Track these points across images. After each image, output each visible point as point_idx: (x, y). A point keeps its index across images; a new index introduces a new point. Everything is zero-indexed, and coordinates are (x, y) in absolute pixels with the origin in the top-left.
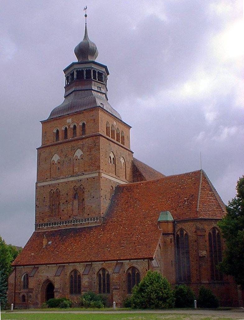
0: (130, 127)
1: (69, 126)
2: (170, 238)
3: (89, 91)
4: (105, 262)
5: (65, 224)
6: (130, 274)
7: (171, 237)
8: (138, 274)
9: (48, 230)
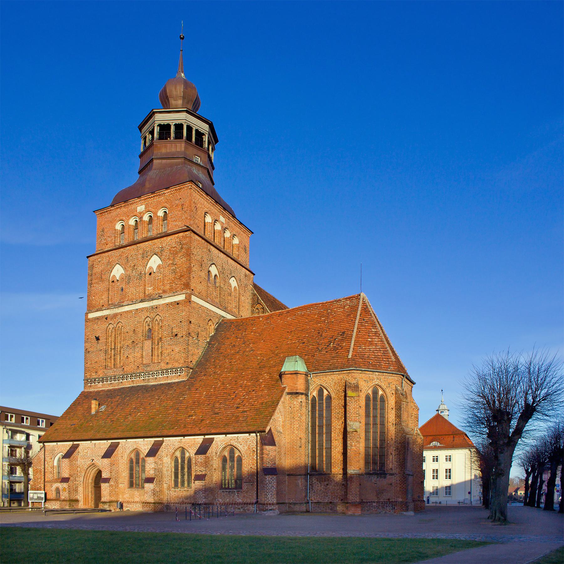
0: (275, 442)
1: (141, 218)
6: (369, 398)
7: (302, 398)
8: (240, 459)
9: (103, 389)
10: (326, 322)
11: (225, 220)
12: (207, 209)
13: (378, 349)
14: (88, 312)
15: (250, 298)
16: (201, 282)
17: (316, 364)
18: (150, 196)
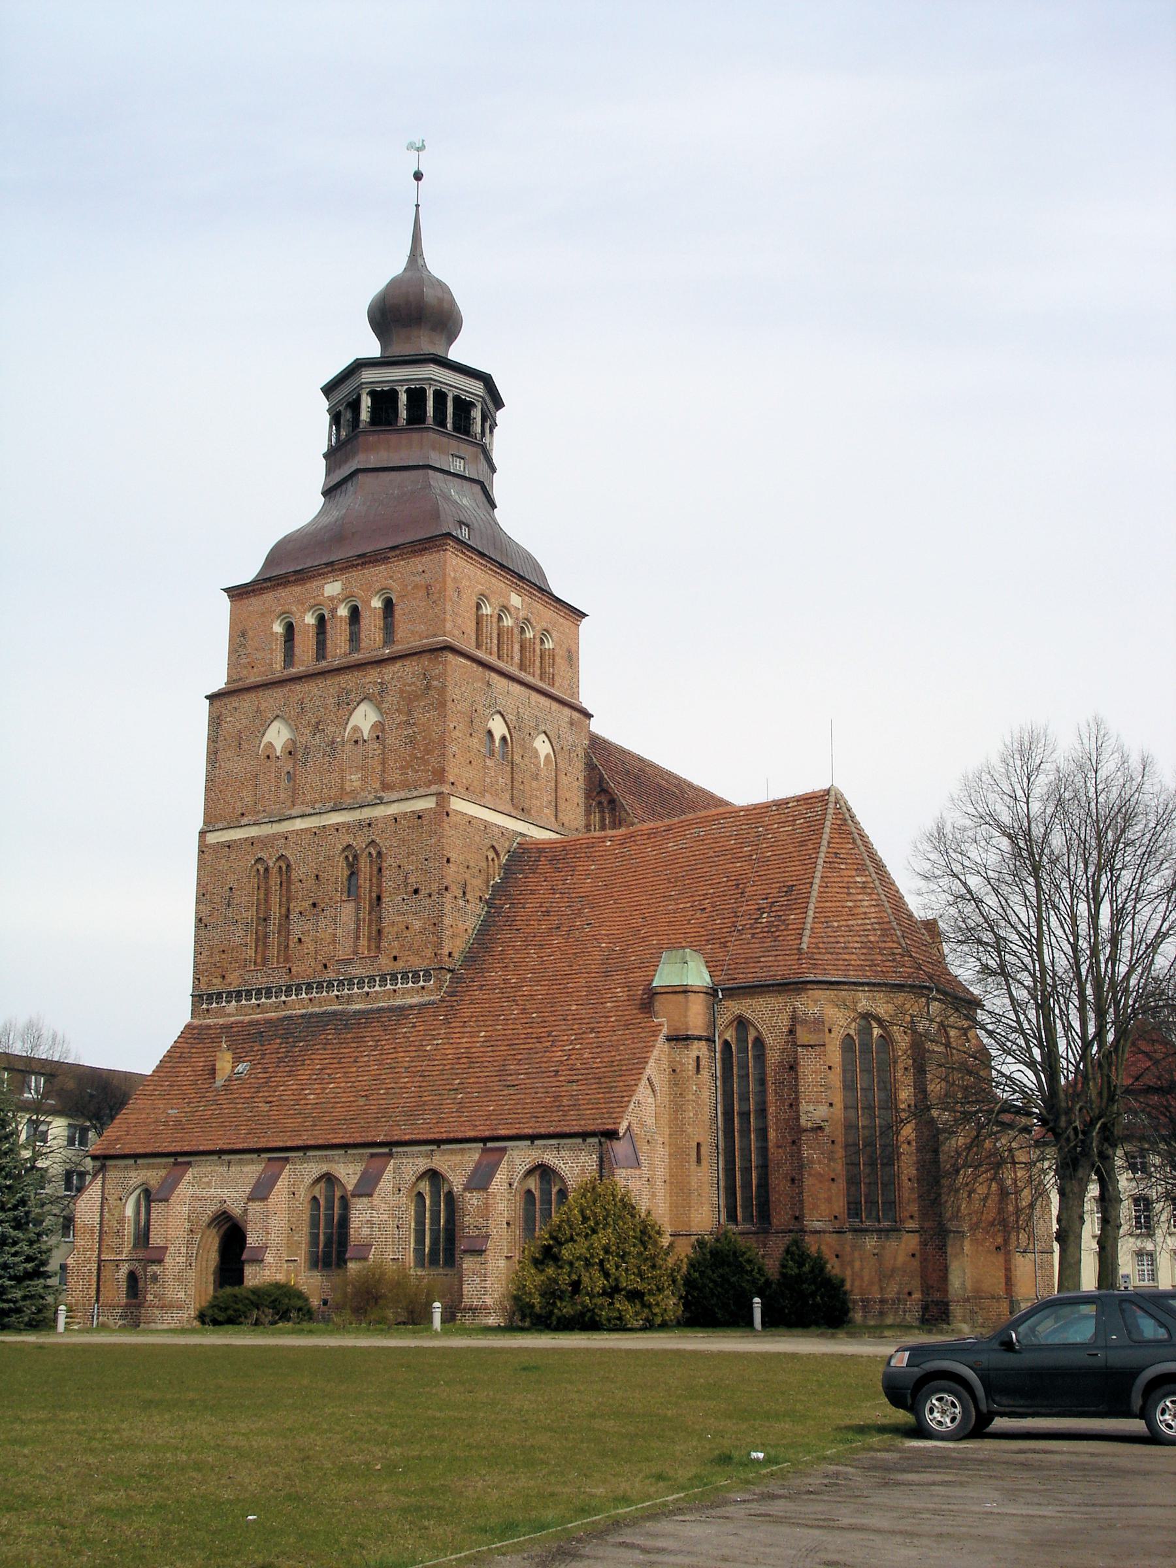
2: (694, 1054)
5: (306, 994)
10: (754, 857)
11: (523, 600)
12: (482, 585)
13: (869, 927)
14: (206, 829)
17: (730, 967)
18: (355, 563)
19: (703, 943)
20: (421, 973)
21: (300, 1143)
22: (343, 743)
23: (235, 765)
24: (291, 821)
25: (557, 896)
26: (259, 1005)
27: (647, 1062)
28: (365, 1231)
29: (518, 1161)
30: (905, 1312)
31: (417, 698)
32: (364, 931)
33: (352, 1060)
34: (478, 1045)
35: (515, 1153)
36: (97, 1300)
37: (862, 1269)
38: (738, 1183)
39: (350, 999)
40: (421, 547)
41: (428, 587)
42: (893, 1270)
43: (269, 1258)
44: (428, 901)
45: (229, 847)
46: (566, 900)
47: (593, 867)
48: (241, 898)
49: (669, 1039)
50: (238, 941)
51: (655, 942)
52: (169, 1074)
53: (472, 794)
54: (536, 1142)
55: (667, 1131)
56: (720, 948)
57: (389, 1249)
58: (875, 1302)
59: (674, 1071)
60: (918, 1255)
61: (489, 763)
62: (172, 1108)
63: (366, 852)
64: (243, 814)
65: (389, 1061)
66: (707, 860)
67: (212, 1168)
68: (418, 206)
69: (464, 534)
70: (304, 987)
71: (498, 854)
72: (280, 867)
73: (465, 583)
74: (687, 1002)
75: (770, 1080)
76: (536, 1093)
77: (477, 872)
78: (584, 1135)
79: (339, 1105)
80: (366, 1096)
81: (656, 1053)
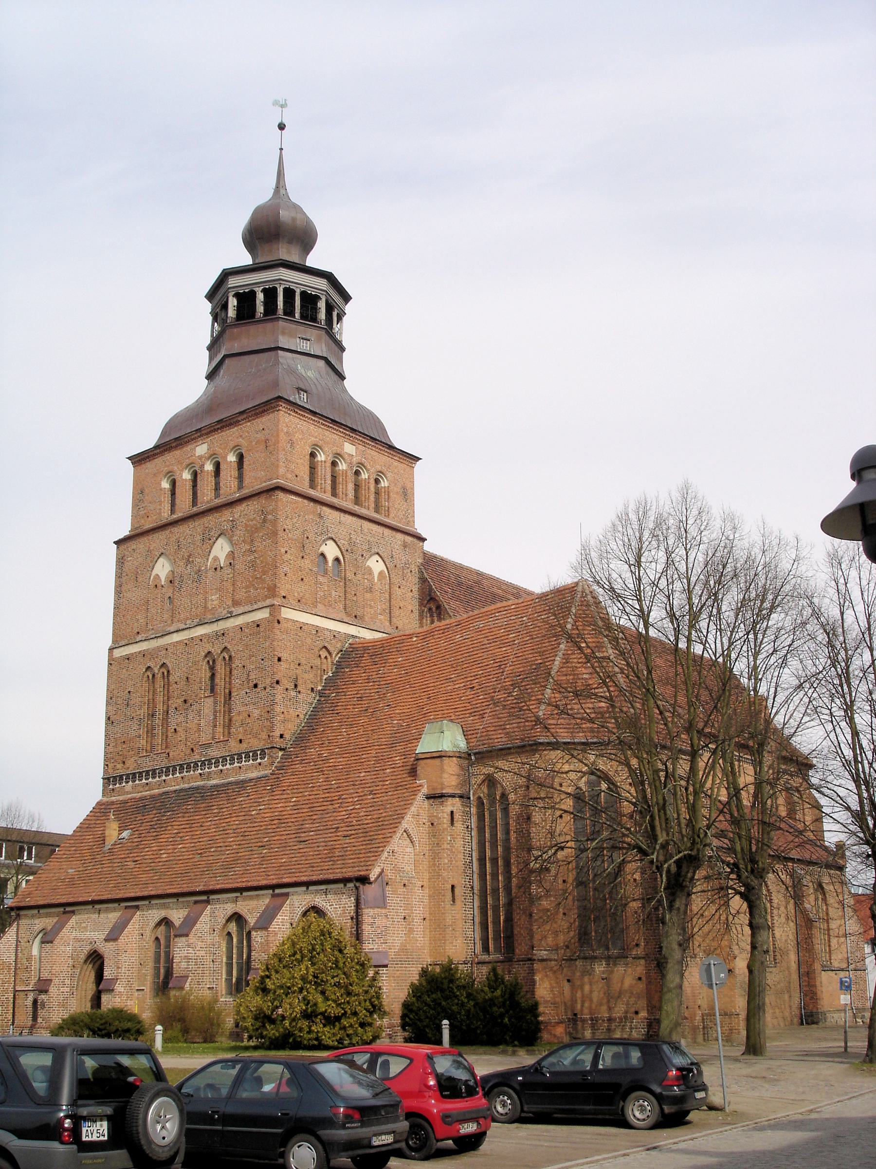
2: (449, 809)
3: (272, 353)
4: (241, 894)
5: (180, 773)
11: (357, 448)
12: (316, 438)
15: (415, 588)
16: (302, 579)
18: (216, 427)
19: (468, 715)
20: (259, 752)
21: (146, 893)
22: (206, 571)
23: (134, 595)
24: (171, 635)
25: (371, 684)
26: (147, 784)
27: (403, 818)
28: (184, 965)
29: (297, 904)
30: (631, 1028)
31: (257, 530)
32: (220, 720)
33: (199, 825)
34: (288, 809)
35: (295, 897)
36: (13, 1023)
37: (591, 992)
38: (490, 919)
39: (209, 776)
40: (261, 410)
41: (266, 441)
42: (620, 993)
43: (119, 988)
44: (264, 693)
45: (128, 659)
46: (377, 687)
47: (400, 659)
48: (136, 700)
49: (429, 797)
50: (134, 734)
51: (432, 717)
52: (77, 842)
53: (301, 604)
54: (311, 888)
55: (427, 876)
56: (479, 719)
57: (207, 979)
58: (604, 1021)
59: (432, 824)
60: (644, 978)
61: (321, 579)
62: (71, 868)
63: (221, 657)
64: (138, 633)
65: (224, 825)
66: (482, 647)
67: (88, 915)
68: (281, 149)
69: (302, 399)
70: (178, 768)
71: (330, 653)
72: (163, 673)
73: (298, 436)
74: (442, 764)
75: (512, 828)
76: (318, 847)
77: (308, 668)
78: (345, 881)
79: (181, 862)
80: (201, 853)
81: (413, 809)
